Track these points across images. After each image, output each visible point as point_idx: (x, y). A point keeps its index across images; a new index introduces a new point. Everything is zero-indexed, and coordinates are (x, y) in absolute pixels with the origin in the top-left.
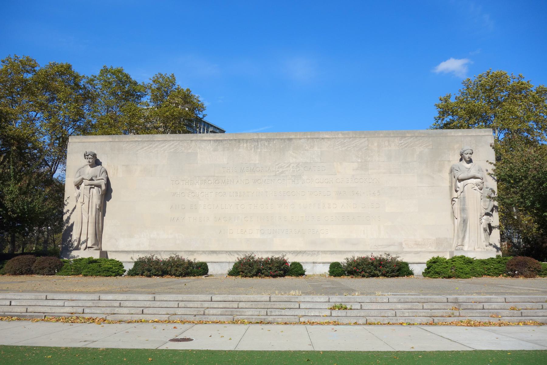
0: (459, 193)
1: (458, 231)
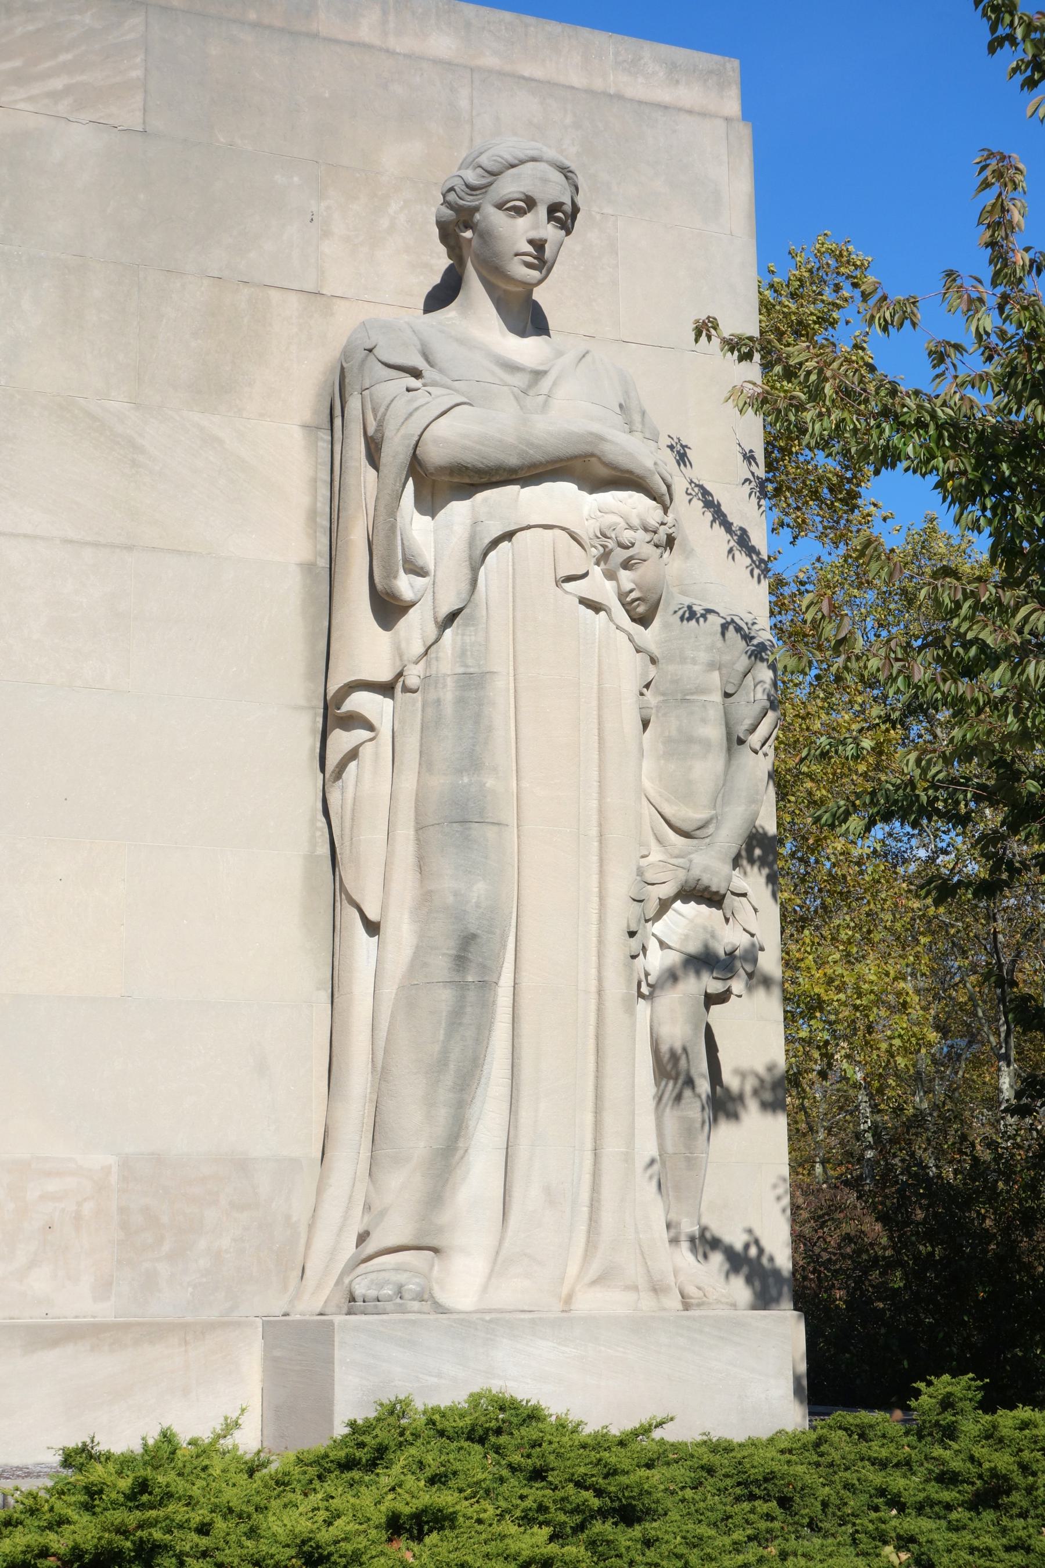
0: (416, 627)
1: (382, 1074)
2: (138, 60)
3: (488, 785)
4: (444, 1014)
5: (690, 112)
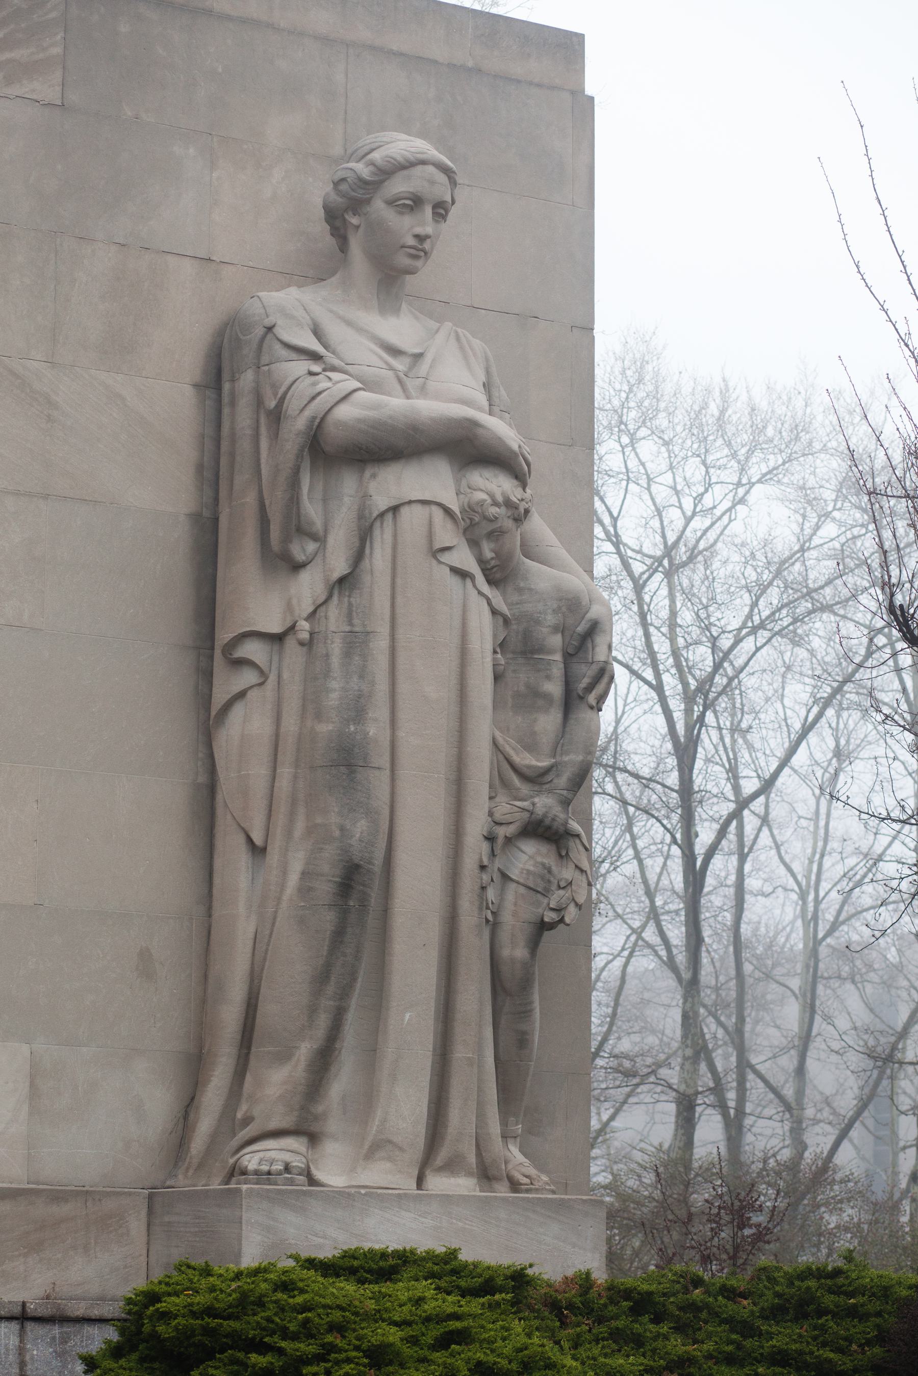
2: (59, 37)
3: (371, 734)
4: (328, 933)
5: (539, 85)
